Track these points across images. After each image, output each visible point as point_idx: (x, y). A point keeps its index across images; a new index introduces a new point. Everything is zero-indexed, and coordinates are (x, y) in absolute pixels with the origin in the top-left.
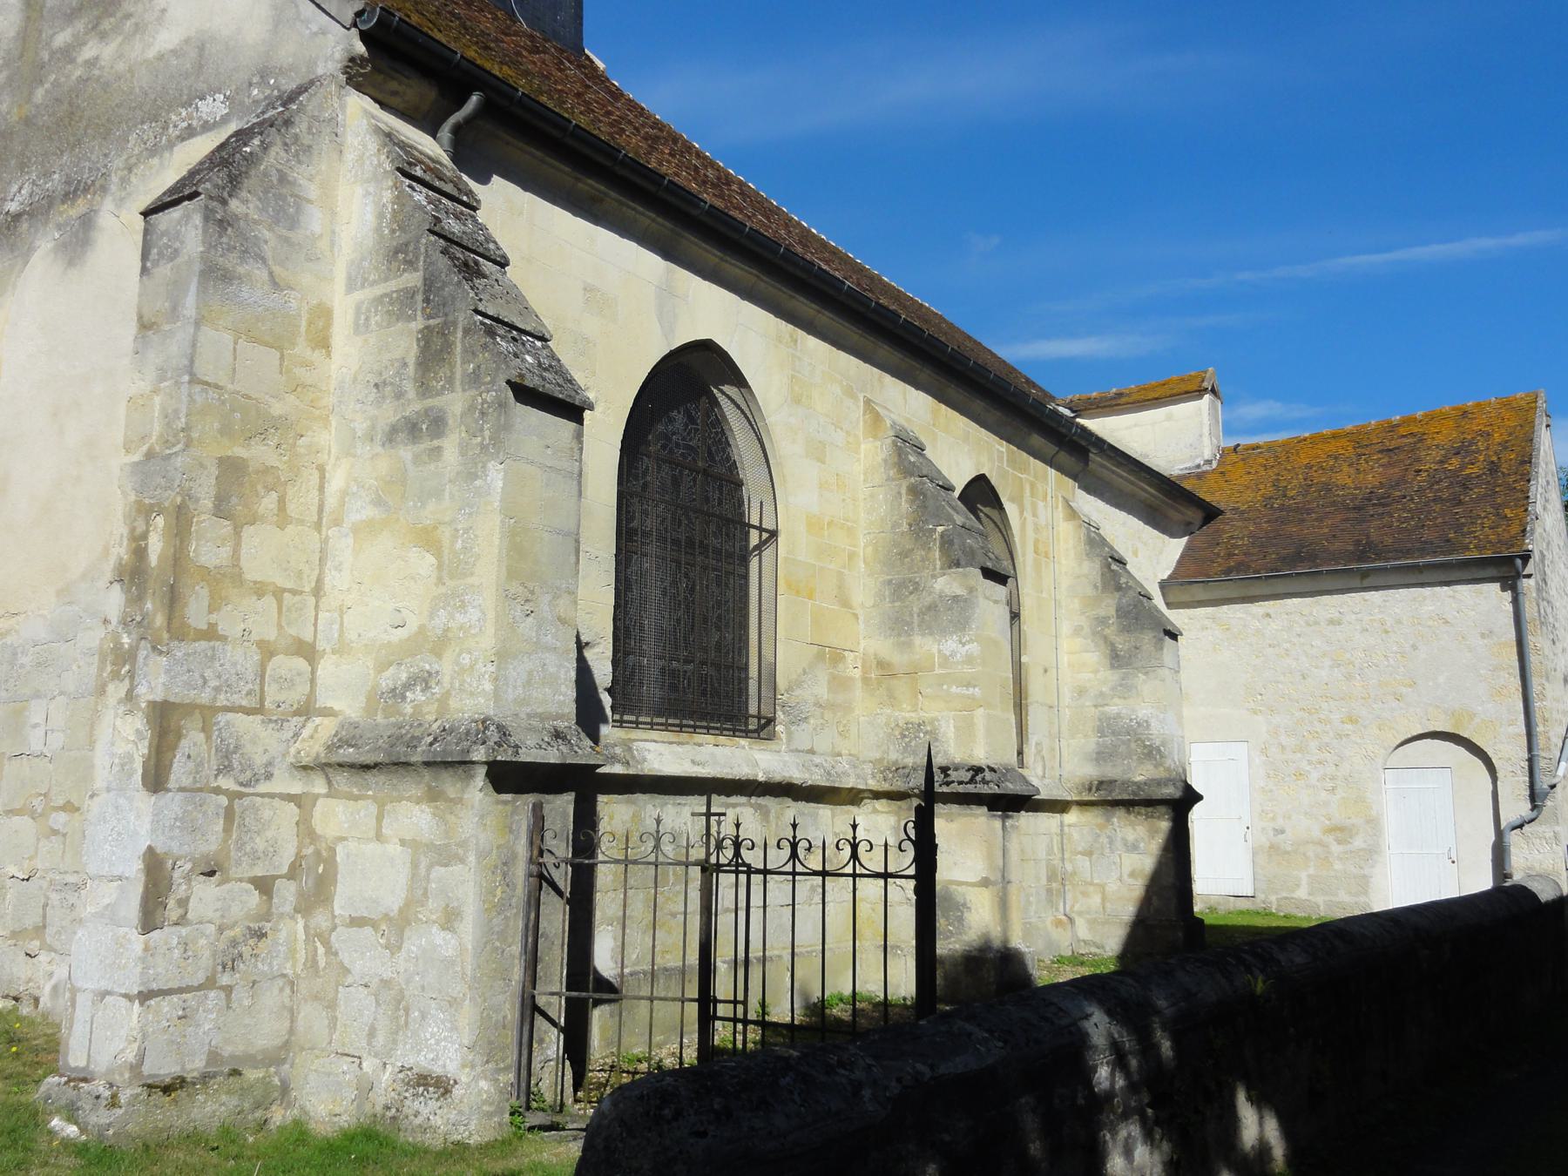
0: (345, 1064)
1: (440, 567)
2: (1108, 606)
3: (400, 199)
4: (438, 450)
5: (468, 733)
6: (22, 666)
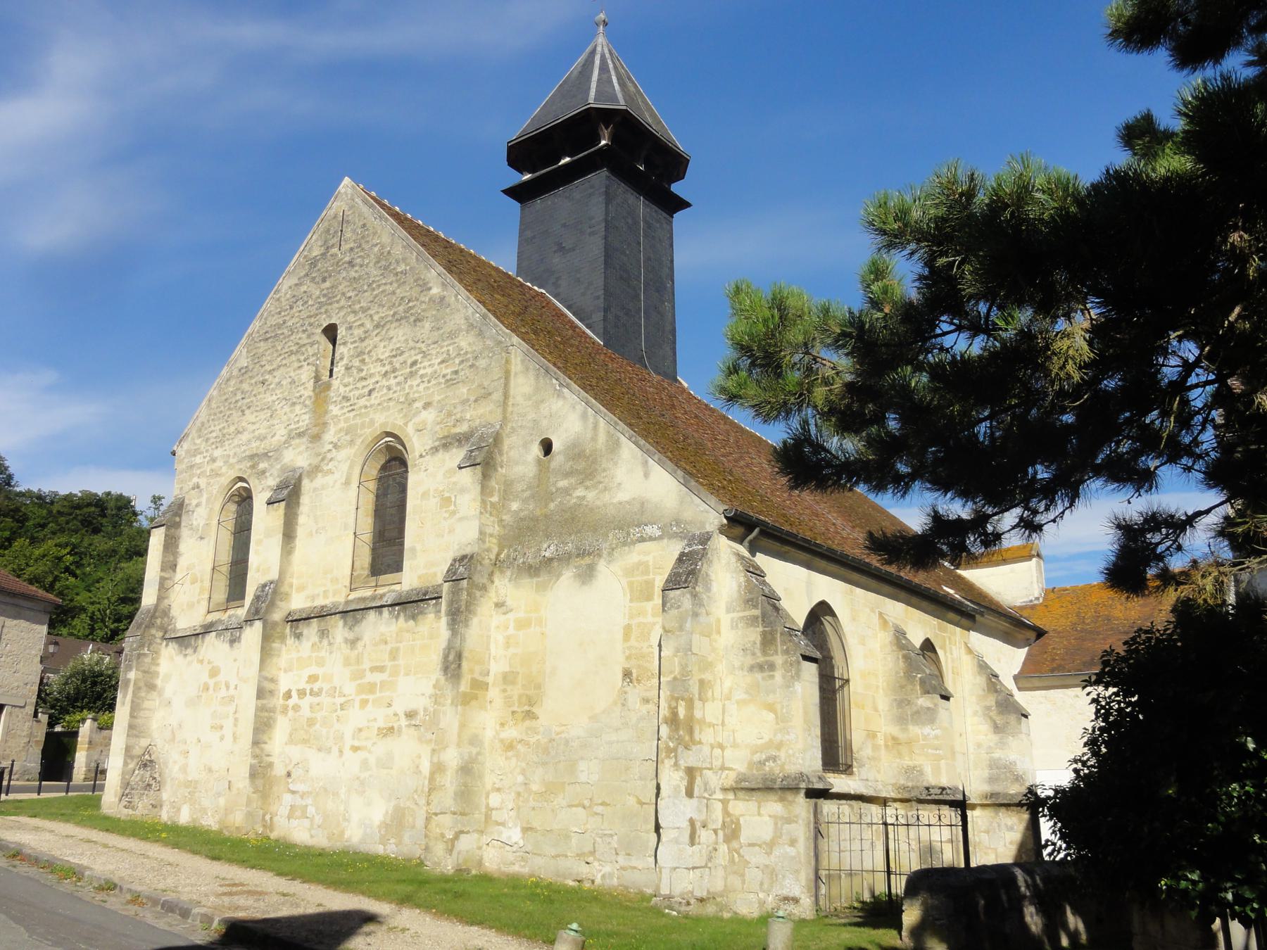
0: (752, 896)
1: (777, 718)
2: (991, 700)
3: (748, 581)
4: (772, 677)
5: (795, 778)
6: (572, 747)
